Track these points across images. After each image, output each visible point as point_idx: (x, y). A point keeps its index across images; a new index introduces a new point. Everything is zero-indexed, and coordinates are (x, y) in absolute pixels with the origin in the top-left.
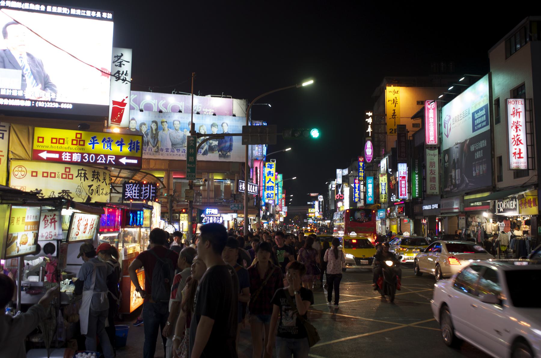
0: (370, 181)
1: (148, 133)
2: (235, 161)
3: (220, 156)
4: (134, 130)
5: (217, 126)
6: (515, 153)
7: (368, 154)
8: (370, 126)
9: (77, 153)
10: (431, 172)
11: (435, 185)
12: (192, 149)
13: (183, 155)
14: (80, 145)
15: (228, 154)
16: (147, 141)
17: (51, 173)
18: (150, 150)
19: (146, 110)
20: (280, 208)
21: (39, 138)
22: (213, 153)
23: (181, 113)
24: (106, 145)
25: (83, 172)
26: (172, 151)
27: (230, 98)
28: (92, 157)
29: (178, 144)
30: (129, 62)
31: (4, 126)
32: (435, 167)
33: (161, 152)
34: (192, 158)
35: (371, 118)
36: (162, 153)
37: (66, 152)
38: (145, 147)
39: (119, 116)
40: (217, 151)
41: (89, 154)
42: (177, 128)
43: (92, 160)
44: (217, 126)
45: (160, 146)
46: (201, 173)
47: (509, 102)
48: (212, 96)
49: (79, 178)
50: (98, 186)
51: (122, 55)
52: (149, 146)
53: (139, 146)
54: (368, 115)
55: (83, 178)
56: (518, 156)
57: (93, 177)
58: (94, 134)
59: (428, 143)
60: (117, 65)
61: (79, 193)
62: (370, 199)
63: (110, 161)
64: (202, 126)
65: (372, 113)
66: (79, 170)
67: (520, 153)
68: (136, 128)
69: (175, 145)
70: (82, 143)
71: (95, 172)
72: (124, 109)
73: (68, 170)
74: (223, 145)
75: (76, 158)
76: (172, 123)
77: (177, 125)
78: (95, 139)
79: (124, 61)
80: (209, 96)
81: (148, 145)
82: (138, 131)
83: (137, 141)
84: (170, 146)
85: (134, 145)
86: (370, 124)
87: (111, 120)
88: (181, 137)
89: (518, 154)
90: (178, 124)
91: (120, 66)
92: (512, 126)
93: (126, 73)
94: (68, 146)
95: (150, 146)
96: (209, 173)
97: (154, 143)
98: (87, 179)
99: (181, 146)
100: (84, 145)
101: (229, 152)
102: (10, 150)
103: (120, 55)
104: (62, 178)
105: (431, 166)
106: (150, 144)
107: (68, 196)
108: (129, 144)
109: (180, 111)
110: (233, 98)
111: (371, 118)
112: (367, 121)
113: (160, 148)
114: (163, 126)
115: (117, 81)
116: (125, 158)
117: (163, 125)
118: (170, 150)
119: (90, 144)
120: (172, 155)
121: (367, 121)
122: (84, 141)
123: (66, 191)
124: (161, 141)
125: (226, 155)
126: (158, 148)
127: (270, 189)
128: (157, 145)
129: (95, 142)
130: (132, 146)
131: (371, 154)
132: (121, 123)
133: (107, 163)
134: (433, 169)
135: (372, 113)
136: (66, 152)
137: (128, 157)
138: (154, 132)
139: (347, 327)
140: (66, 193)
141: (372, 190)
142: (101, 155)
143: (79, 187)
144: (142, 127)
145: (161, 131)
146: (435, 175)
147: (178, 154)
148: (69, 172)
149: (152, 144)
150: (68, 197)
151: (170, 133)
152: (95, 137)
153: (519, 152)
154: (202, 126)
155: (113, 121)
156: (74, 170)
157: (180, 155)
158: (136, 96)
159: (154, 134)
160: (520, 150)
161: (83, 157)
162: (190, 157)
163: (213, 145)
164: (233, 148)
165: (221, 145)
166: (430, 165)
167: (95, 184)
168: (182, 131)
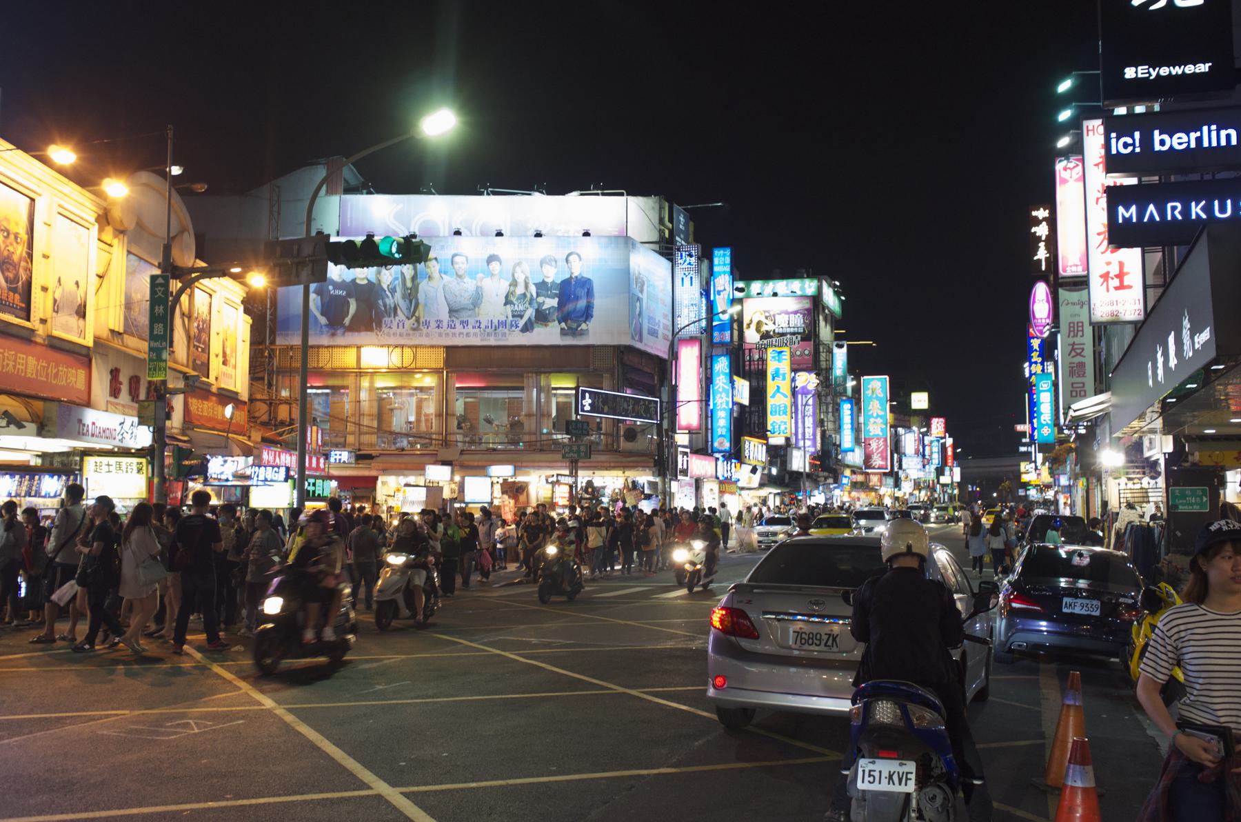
0: (1044, 386)
1: (395, 287)
2: (599, 343)
3: (563, 333)
4: (365, 282)
6: (1106, 276)
7: (1037, 315)
8: (1042, 245)
10: (1073, 349)
11: (1084, 384)
12: (159, 306)
13: (475, 335)
15: (584, 326)
16: (393, 306)
18: (401, 325)
20: (882, 460)
22: (546, 325)
26: (449, 326)
27: (622, 194)
29: (463, 309)
32: (1083, 336)
33: (425, 331)
34: (161, 325)
35: (1044, 223)
38: (390, 319)
40: (557, 322)
42: (460, 273)
44: (556, 262)
46: (522, 376)
47: (1088, 131)
48: (582, 195)
54: (1036, 217)
56: (1116, 282)
59: (1065, 271)
62: (1046, 431)
64: (519, 264)
65: (1047, 211)
67: (1120, 276)
69: (456, 311)
74: (570, 307)
77: (461, 265)
80: (575, 194)
84: (445, 316)
86: (1043, 238)
88: (470, 293)
89: (1117, 276)
90: (463, 263)
92: (1098, 199)
95: (401, 316)
96: (539, 373)
97: (409, 309)
99: (470, 313)
101: (585, 322)
105: (1072, 334)
109: (499, 234)
110: (627, 195)
111: (1044, 223)
112: (1035, 233)
113: (422, 320)
114: (428, 270)
117: (429, 267)
118: (445, 324)
120: (451, 335)
121: (1035, 233)
124: (426, 305)
126: (418, 320)
127: (780, 411)
128: (417, 314)
131: (1048, 317)
134: (1077, 340)
135: (1047, 211)
138: (409, 284)
141: (1050, 408)
144: (382, 274)
145: (426, 281)
146: (1084, 357)
147: (465, 331)
149: (405, 311)
151: (444, 286)
153: (1117, 272)
154: (519, 264)
158: (401, 206)
159: (408, 289)
160: (1121, 265)
162: (156, 325)
164: (596, 312)
165: (565, 306)
166: (1070, 331)
168: (471, 278)
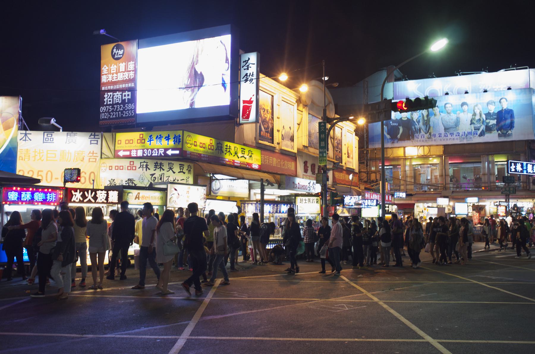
3: (499, 136)
4: (406, 119)
5: (494, 103)
9: (140, 149)
13: (457, 139)
14: (142, 143)
15: (510, 132)
16: (419, 128)
17: (120, 166)
18: (423, 137)
19: (473, 92)
21: (118, 141)
22: (491, 133)
23: (510, 90)
24: (158, 140)
25: (145, 164)
27: (526, 68)
28: (149, 151)
29: (451, 128)
30: (254, 64)
31: (98, 135)
33: (434, 138)
34: (323, 142)
36: (435, 138)
37: (134, 150)
38: (418, 134)
39: (248, 113)
40: (496, 131)
41: (147, 150)
43: (149, 154)
45: (432, 131)
48: (506, 71)
49: (141, 169)
50: (162, 174)
51: (249, 59)
52: (421, 134)
53: (180, 139)
55: (145, 169)
57: (156, 168)
58: (150, 133)
60: (245, 68)
61: (142, 181)
63: (161, 153)
66: (141, 163)
68: (408, 117)
69: (448, 129)
70: (143, 141)
71: (158, 164)
72: (251, 106)
73: (132, 163)
74: (503, 123)
75: (140, 154)
76: (444, 107)
77: (449, 108)
78: (151, 137)
79: (250, 64)
80: (502, 70)
81: (420, 132)
82: (410, 119)
83: (179, 135)
84: (442, 131)
85: (177, 139)
87: (242, 117)
91: (248, 69)
93: (253, 74)
94: (136, 145)
95: (422, 132)
96: (488, 155)
97: (426, 129)
98: (149, 169)
99: (454, 129)
100: (144, 143)
102: (103, 152)
103: (248, 59)
104: (128, 169)
106: (422, 131)
107: (133, 183)
108: (173, 138)
109: (466, 93)
110: (529, 68)
113: (432, 134)
114: (434, 112)
115: (245, 82)
116: (171, 150)
117: (434, 110)
118: (443, 135)
119: (148, 141)
120: (445, 140)
122: (144, 140)
123: (131, 179)
124: (433, 127)
125: (506, 133)
126: (430, 134)
128: (430, 131)
129: (151, 139)
130: (176, 140)
132: (250, 118)
133: (159, 155)
136: (134, 150)
137: (173, 149)
138: (426, 118)
139: (258, 264)
140: (131, 181)
142: (155, 150)
143: (141, 176)
144: (413, 115)
145: (433, 117)
147: (452, 138)
148: (133, 165)
149: (425, 131)
150: (132, 184)
151: (442, 118)
152: (151, 136)
154: (477, 105)
155: (244, 118)
156: (137, 163)
157: (453, 139)
159: (425, 121)
161: (144, 153)
163: (490, 124)
164: (515, 125)
167: (158, 173)
168: (454, 114)
